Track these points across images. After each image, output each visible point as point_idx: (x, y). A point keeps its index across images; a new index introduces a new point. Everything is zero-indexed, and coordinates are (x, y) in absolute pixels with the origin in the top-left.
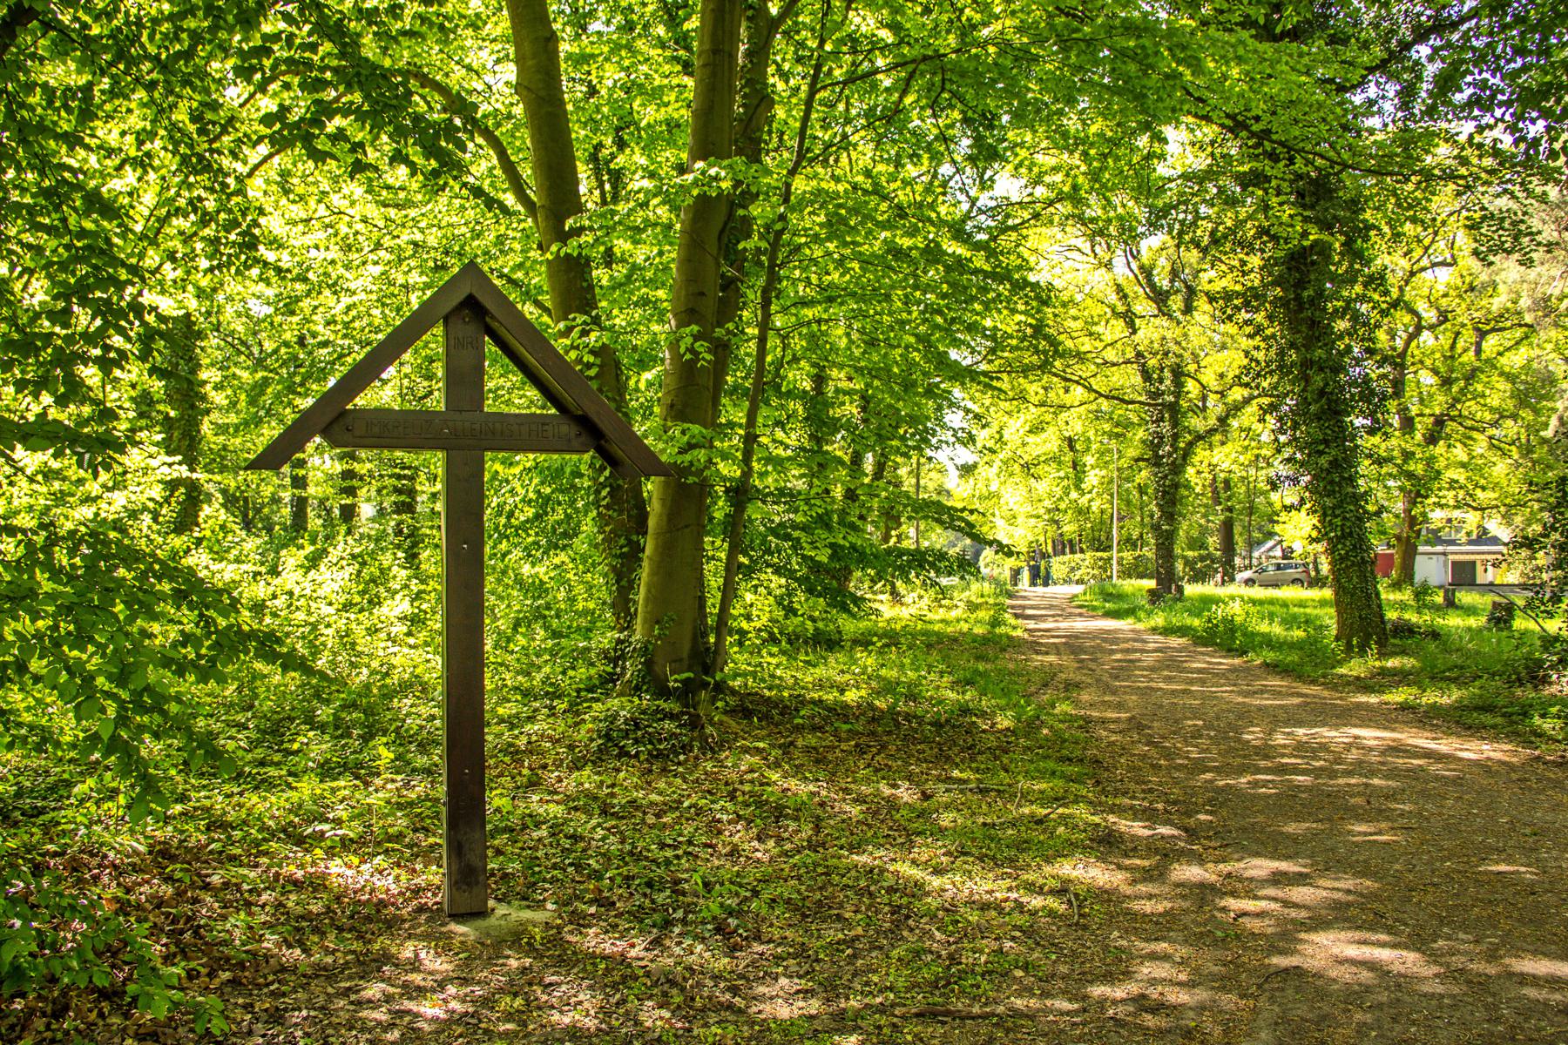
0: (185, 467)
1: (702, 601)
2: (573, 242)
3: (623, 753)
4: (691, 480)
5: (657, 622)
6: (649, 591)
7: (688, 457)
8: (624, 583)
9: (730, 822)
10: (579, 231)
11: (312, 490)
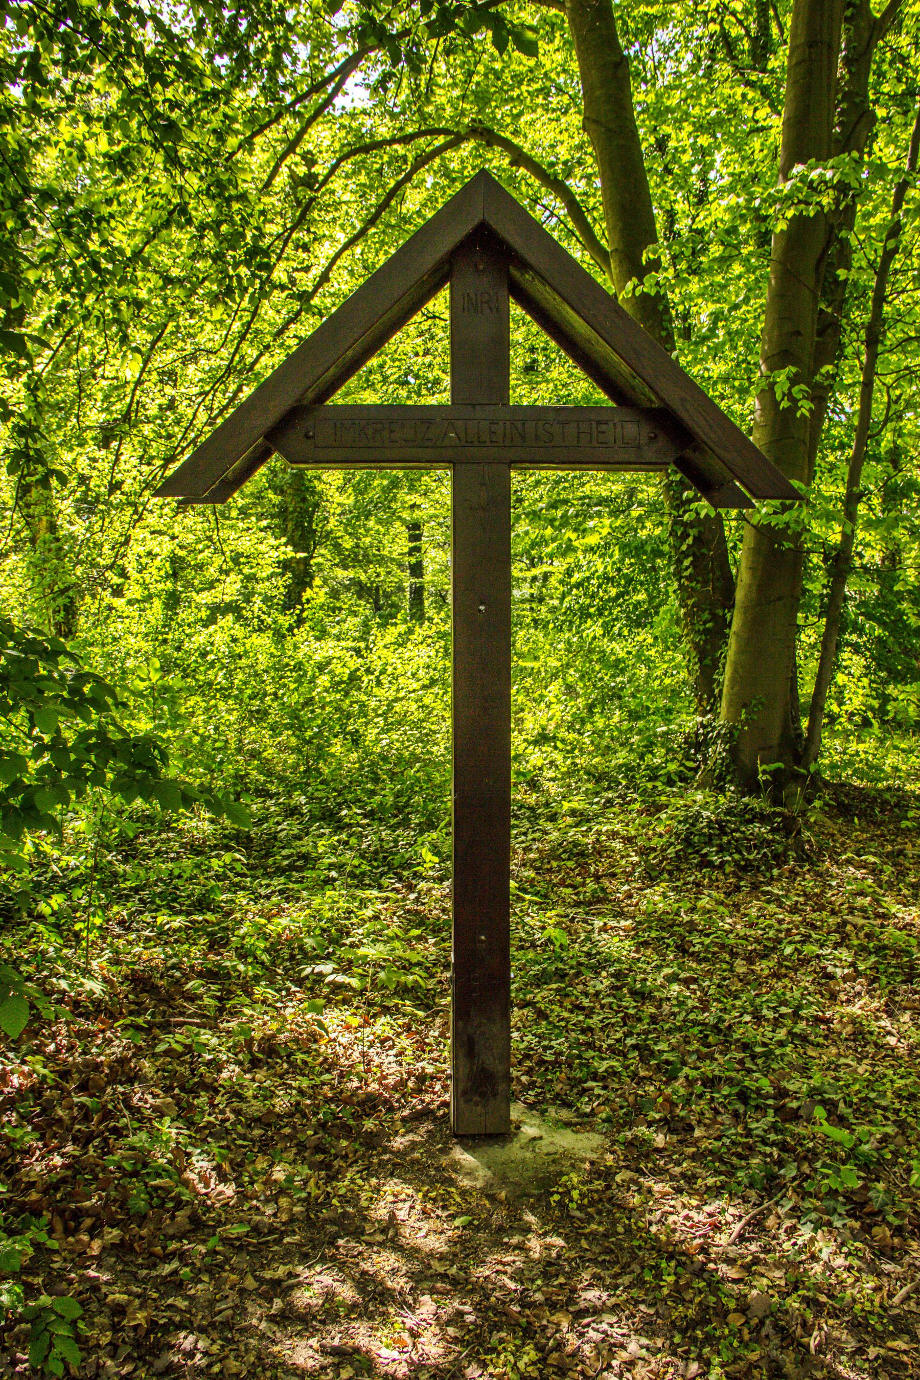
0: (290, 548)
1: (793, 689)
2: (649, 280)
3: (705, 863)
4: (787, 545)
5: (745, 706)
6: (735, 671)
7: (786, 517)
8: (707, 662)
9: (845, 979)
10: (656, 265)
11: (428, 578)
